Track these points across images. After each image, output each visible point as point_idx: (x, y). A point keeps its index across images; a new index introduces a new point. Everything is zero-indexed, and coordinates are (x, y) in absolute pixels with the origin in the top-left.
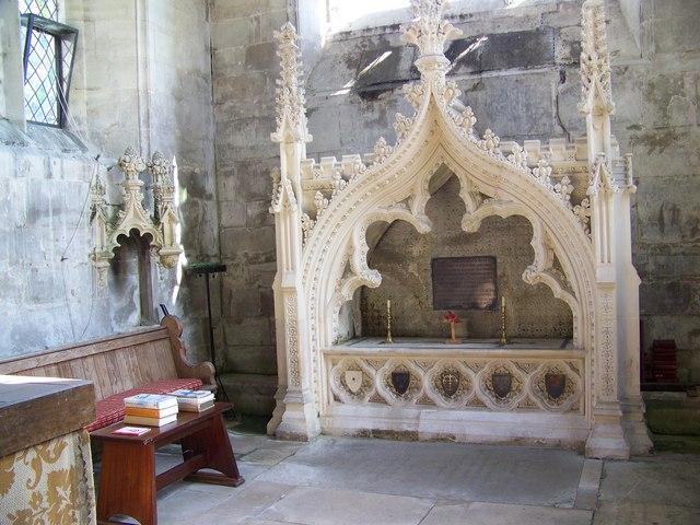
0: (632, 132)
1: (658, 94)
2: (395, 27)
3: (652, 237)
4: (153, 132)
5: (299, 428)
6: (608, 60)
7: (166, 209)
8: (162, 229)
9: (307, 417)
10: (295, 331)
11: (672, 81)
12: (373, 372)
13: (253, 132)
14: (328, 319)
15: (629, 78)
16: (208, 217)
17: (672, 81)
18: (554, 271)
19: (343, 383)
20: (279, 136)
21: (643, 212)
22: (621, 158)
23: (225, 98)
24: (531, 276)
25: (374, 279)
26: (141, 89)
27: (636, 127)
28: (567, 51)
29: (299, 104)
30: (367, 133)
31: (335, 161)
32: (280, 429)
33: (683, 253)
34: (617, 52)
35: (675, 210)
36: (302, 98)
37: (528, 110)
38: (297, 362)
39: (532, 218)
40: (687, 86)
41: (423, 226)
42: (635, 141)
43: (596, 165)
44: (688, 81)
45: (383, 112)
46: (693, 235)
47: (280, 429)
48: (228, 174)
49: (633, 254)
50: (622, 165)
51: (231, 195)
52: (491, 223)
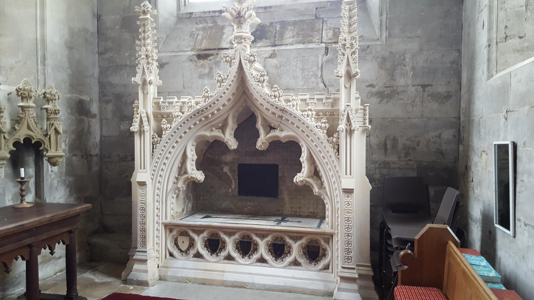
0: (369, 89)
1: (388, 65)
2: (221, 12)
3: (376, 157)
4: (49, 70)
5: (142, 277)
6: (357, 42)
7: (53, 125)
8: (50, 139)
9: (149, 268)
10: (144, 209)
11: (397, 56)
12: (195, 236)
13: (126, 75)
14: (169, 203)
15: (370, 53)
16: (92, 130)
17: (397, 56)
18: (315, 177)
19: (176, 244)
20: (137, 79)
21: (374, 141)
22: (362, 107)
23: (106, 50)
24: (299, 178)
25: (200, 176)
26: (39, 38)
27: (371, 86)
28: (331, 34)
29: (153, 60)
30: (200, 81)
31: (52, 92)
32: (129, 277)
33: (399, 168)
34: (362, 36)
35: (395, 140)
36: (155, 55)
37: (303, 72)
38: (144, 230)
39: (302, 143)
40: (407, 60)
41: (233, 144)
42: (372, 94)
43: (344, 111)
44: (408, 56)
45: (211, 69)
46: (406, 157)
47: (129, 277)
48: (107, 102)
49: (366, 167)
50: (362, 111)
51: (110, 116)
52: (275, 144)
